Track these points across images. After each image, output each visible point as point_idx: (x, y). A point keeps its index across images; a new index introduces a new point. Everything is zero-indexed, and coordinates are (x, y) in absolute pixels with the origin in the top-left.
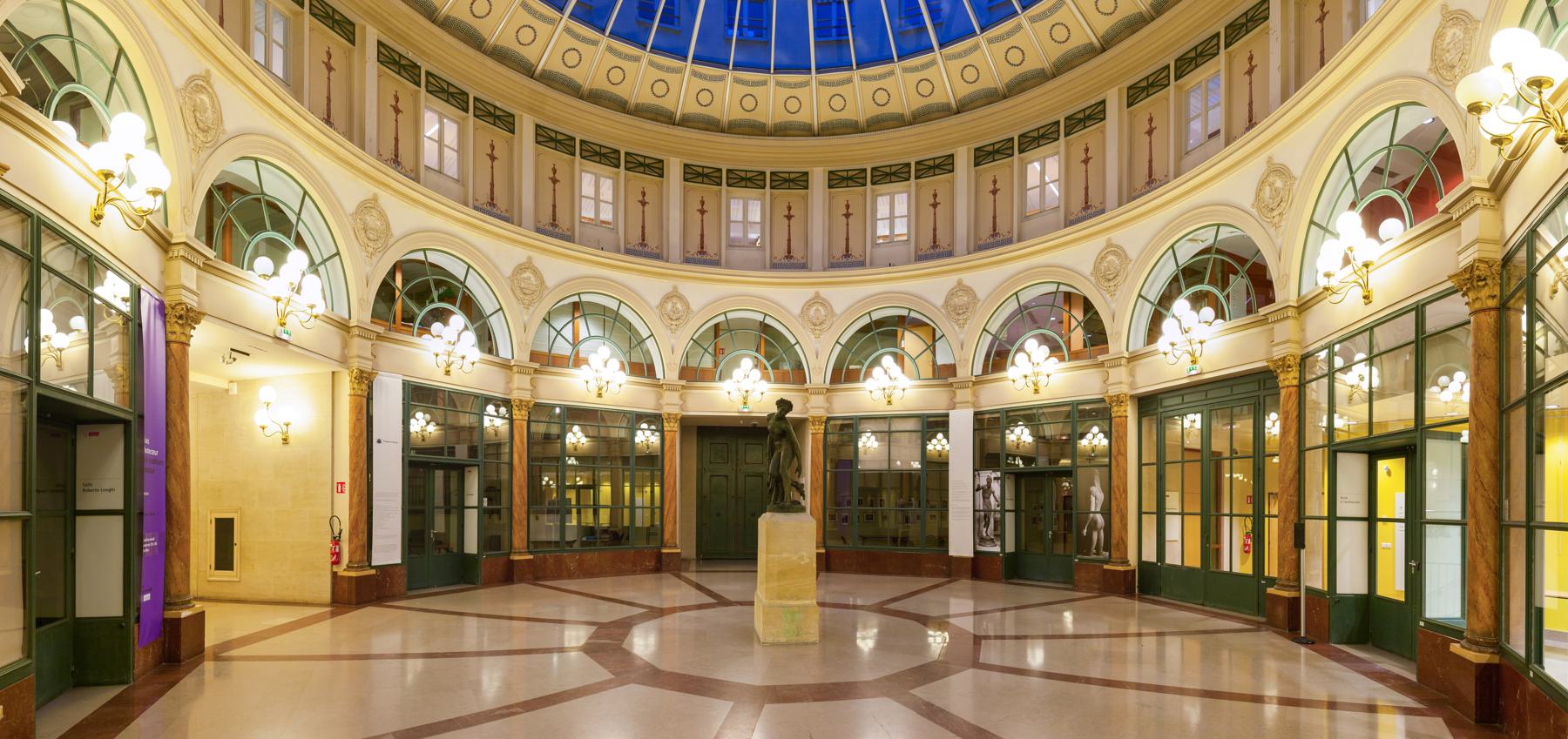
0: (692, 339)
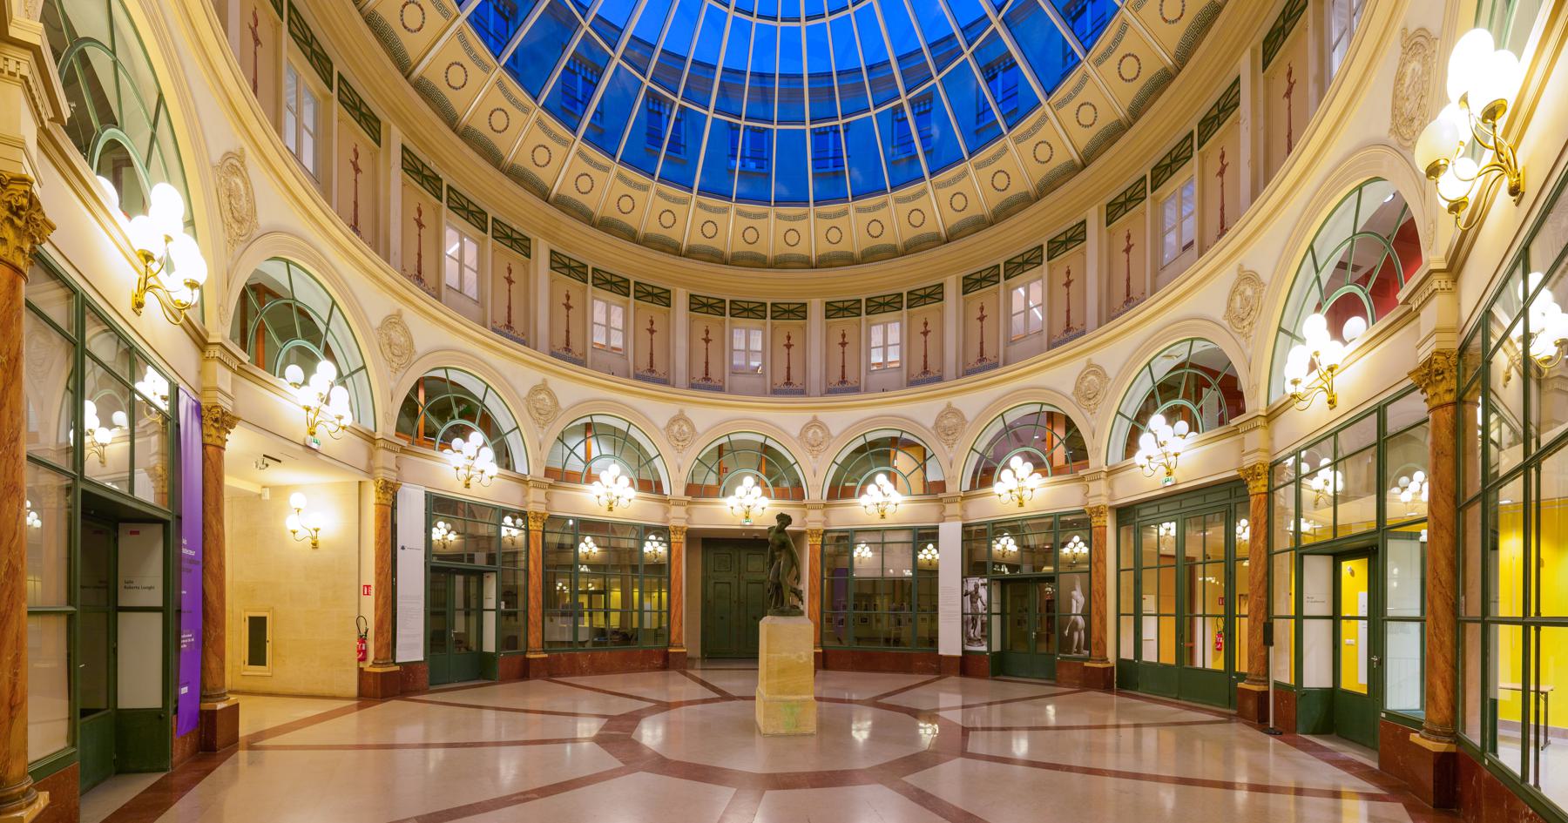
0: (697, 458)
